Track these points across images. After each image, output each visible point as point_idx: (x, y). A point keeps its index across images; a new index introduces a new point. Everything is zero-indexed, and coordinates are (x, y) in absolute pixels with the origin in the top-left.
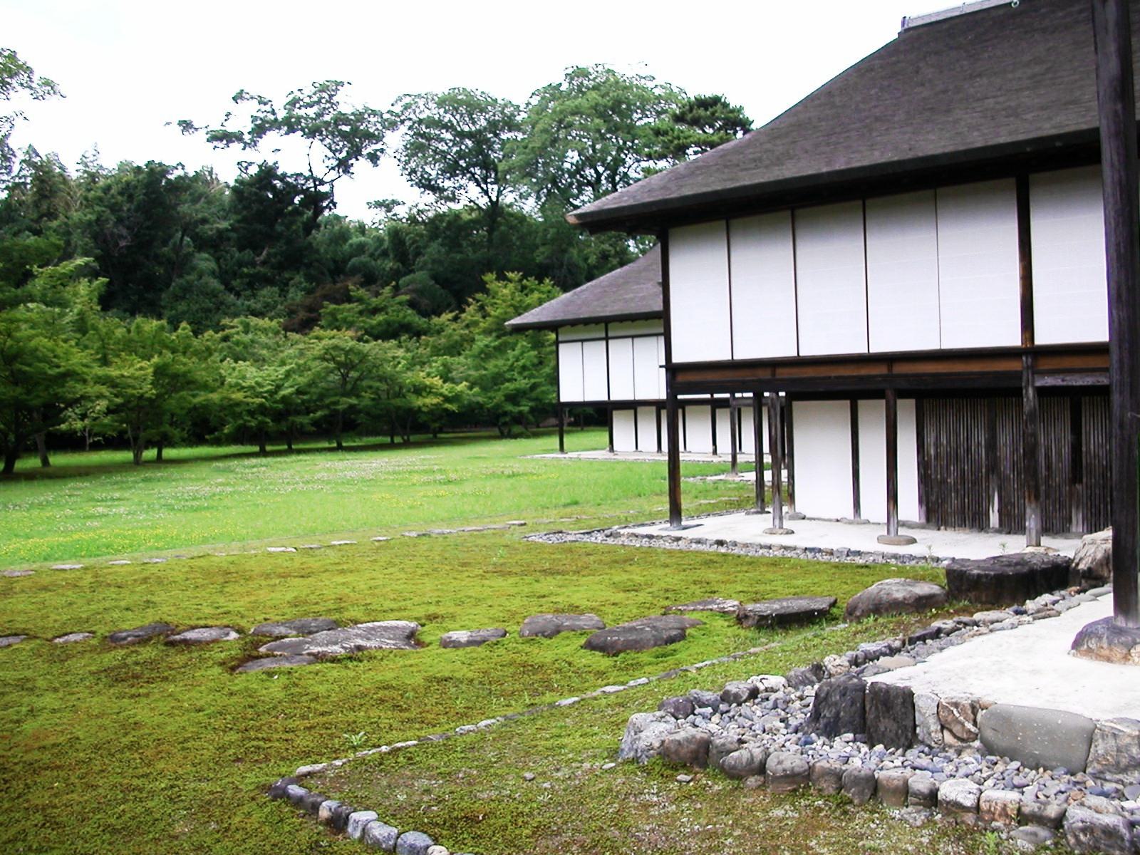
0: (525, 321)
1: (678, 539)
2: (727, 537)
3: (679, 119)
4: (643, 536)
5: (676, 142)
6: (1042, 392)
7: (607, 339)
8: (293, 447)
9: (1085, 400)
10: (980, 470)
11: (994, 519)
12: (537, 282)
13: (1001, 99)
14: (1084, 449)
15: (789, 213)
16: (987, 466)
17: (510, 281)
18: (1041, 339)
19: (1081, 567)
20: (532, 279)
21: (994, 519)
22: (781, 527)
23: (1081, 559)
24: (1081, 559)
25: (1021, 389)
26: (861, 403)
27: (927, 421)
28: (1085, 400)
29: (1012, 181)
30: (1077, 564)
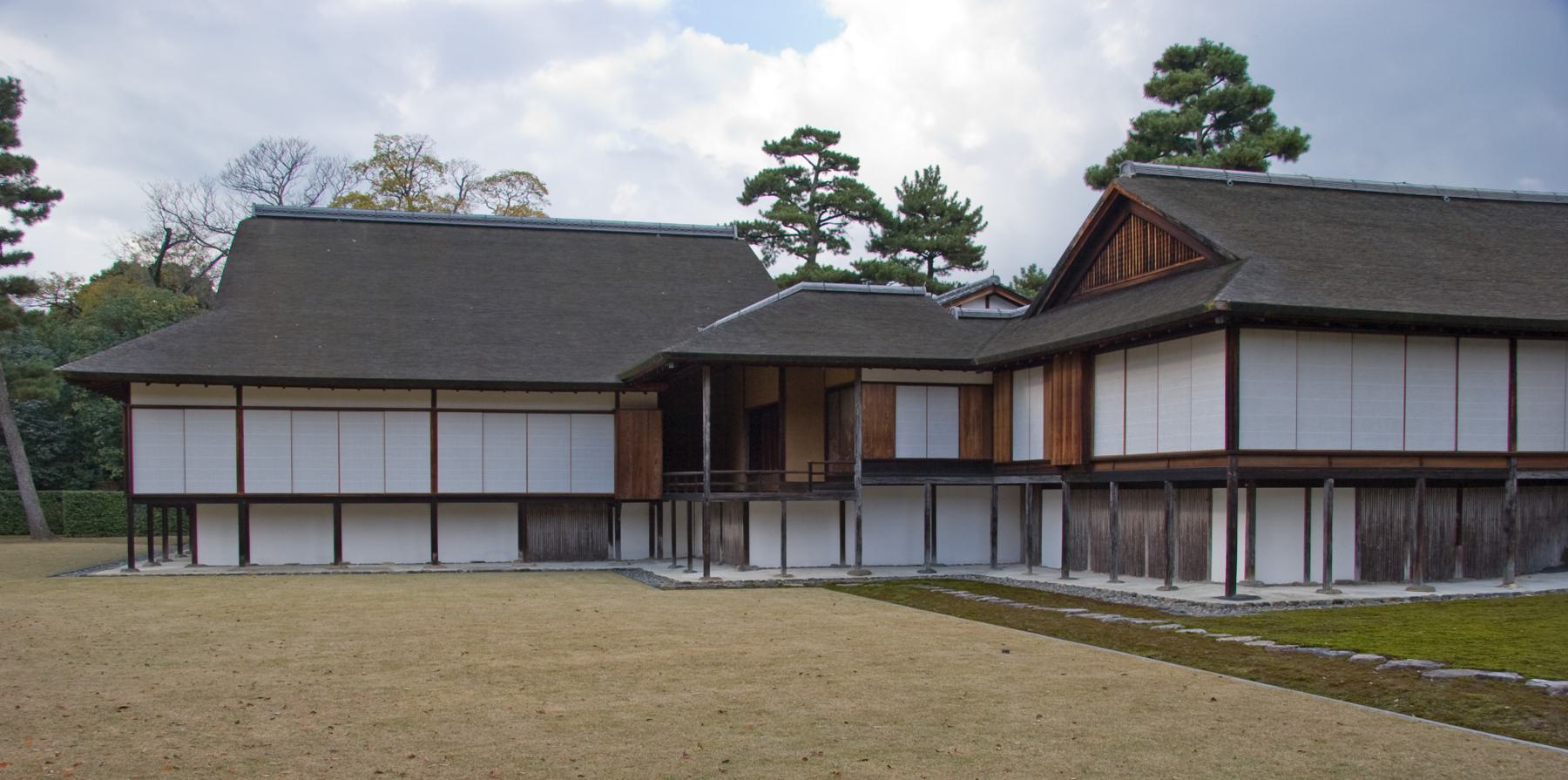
6: (1521, 483)
18: (1527, 443)
21: (1407, 573)
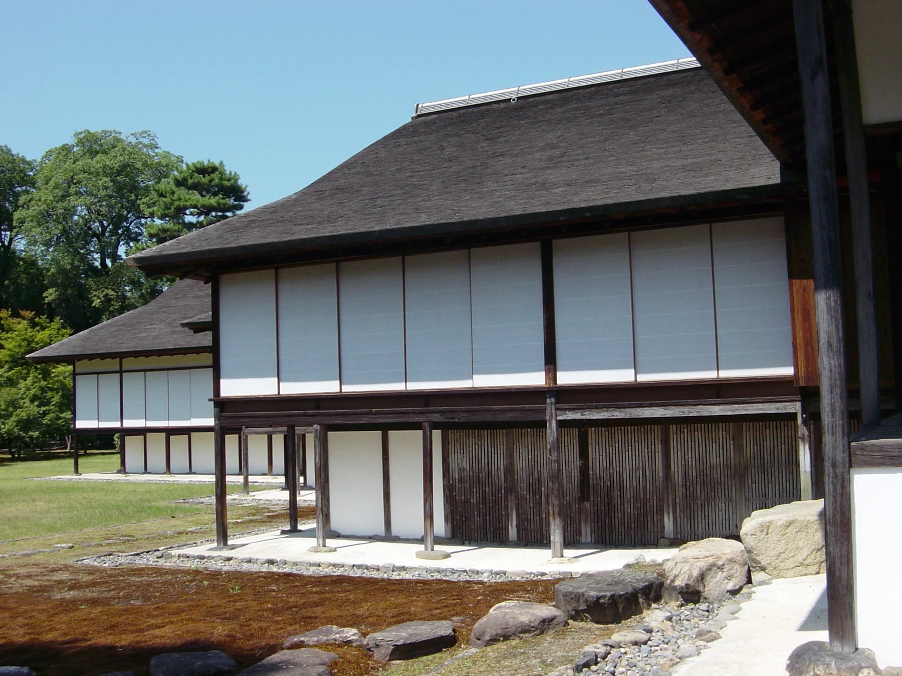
0: (45, 354)
1: (229, 559)
2: (277, 557)
3: (180, 183)
4: (195, 558)
5: (176, 203)
6: (562, 424)
7: (121, 372)
8: (300, 527)
9: (591, 431)
10: (499, 491)
11: (513, 533)
12: (48, 321)
13: (528, 175)
14: (591, 472)
15: (273, 271)
16: (506, 488)
17: (24, 318)
19: (678, 583)
20: (44, 317)
21: (513, 533)
22: (324, 546)
23: (676, 576)
24: (676, 576)
25: (545, 422)
26: (392, 433)
27: (451, 448)
28: (591, 431)
29: (536, 246)
30: (673, 581)
